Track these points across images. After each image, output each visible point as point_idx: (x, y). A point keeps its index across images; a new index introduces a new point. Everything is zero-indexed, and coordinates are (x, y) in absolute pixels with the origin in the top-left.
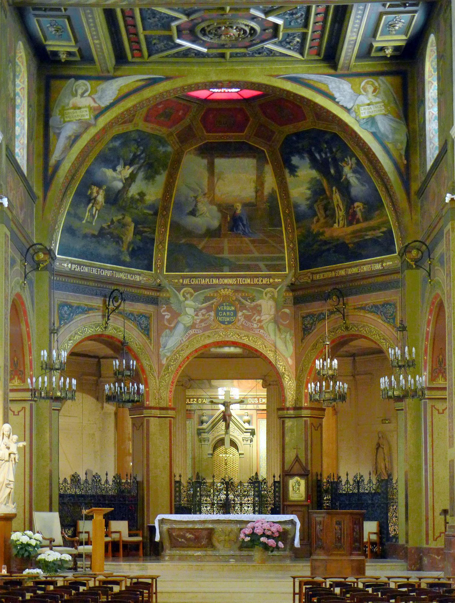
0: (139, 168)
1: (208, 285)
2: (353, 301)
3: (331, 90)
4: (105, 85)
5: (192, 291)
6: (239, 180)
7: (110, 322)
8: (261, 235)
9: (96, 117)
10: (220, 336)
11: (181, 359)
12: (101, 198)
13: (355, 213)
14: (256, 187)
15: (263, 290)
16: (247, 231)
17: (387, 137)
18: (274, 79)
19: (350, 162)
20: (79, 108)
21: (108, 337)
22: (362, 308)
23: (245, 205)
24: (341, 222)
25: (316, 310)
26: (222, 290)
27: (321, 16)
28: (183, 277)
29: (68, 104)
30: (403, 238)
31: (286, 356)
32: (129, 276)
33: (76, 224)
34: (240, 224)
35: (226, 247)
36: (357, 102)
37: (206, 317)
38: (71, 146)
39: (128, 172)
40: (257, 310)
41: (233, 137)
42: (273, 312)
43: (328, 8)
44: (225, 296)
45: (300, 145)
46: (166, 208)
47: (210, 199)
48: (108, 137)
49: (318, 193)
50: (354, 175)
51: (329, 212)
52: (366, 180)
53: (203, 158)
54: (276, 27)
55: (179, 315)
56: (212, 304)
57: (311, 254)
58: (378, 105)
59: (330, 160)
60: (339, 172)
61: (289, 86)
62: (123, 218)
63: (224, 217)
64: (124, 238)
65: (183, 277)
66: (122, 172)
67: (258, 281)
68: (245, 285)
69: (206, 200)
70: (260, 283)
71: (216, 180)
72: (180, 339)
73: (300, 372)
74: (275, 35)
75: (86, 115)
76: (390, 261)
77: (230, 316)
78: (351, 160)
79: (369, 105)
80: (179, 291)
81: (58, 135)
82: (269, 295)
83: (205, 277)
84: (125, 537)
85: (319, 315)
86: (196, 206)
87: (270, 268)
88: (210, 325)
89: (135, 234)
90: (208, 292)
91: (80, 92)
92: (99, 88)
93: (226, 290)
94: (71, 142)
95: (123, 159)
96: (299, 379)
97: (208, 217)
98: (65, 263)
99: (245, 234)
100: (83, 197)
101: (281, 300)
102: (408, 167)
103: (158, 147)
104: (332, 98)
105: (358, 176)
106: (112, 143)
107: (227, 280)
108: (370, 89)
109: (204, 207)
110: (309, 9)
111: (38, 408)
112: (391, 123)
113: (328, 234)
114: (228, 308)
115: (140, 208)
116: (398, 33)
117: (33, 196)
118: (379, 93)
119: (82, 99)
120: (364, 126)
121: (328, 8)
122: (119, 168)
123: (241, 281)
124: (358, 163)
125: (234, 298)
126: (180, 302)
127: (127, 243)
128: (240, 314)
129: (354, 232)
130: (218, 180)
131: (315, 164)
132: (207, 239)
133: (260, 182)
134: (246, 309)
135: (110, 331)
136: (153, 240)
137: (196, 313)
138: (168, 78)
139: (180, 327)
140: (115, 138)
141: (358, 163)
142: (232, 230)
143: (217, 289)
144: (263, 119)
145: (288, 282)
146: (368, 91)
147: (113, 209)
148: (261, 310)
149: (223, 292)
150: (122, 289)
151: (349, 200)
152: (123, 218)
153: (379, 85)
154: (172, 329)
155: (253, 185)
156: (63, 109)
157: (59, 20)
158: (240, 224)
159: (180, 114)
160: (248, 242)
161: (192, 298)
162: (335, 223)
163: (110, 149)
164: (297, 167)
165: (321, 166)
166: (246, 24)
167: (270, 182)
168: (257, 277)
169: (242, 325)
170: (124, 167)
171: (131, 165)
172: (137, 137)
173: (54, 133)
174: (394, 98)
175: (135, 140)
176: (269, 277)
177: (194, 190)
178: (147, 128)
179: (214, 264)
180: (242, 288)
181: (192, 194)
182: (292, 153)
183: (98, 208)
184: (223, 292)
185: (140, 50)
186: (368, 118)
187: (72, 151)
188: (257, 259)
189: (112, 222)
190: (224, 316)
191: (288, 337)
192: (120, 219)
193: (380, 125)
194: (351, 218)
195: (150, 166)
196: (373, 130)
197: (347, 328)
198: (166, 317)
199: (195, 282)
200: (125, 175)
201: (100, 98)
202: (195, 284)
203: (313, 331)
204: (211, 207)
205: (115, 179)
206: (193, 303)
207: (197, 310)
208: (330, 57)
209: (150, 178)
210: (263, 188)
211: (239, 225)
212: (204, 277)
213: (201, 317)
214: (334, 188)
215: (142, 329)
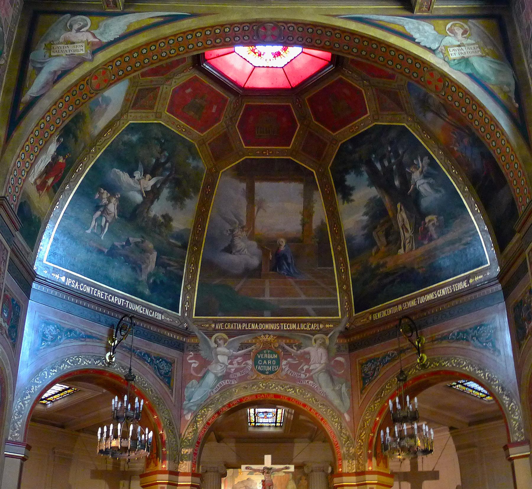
0: (164, 183)
1: (245, 330)
3: (408, 31)
5: (225, 336)
8: (309, 275)
10: (260, 387)
12: (112, 208)
14: (303, 220)
15: (311, 336)
16: (292, 271)
17: (489, 79)
18: (334, 19)
19: (421, 165)
20: (73, 43)
21: (112, 375)
23: (290, 241)
24: (407, 246)
25: (378, 353)
26: (262, 336)
28: (216, 322)
29: (58, 39)
31: (342, 411)
32: (147, 311)
34: (285, 263)
35: (268, 292)
36: (443, 43)
37: (242, 365)
38: (55, 82)
39: (149, 183)
40: (306, 358)
42: (324, 360)
44: (265, 343)
45: (356, 156)
46: (197, 243)
47: (248, 234)
49: (378, 214)
50: (426, 181)
51: (393, 237)
53: (241, 181)
56: (250, 351)
58: (472, 46)
59: (394, 167)
60: (406, 181)
61: (353, 26)
62: (143, 242)
63: (265, 254)
64: (143, 266)
65: (216, 322)
66: (142, 181)
67: (306, 327)
68: (290, 330)
69: (244, 234)
70: (308, 328)
71: (256, 209)
72: (210, 390)
73: (360, 429)
75: (81, 50)
77: (272, 365)
78: (422, 161)
79: (459, 46)
80: (210, 337)
81: (40, 70)
82: (318, 342)
83: (241, 322)
85: (384, 358)
86: (232, 241)
88: (248, 374)
90: (246, 338)
91: (76, 27)
92: (102, 25)
93: (267, 336)
94: (56, 78)
95: (143, 163)
97: (247, 254)
99: (289, 274)
101: (334, 348)
103: (187, 158)
104: (411, 39)
105: (431, 181)
106: (128, 135)
108: (460, 32)
109: (241, 243)
112: (491, 65)
113: (391, 264)
114: (270, 356)
115: (164, 234)
118: (471, 35)
119: (78, 33)
120: (457, 67)
122: (138, 175)
123: (285, 327)
125: (277, 345)
127: (147, 273)
128: (284, 362)
130: (258, 210)
131: (376, 179)
132: (244, 280)
133: (307, 214)
134: (292, 357)
137: (229, 361)
138: (193, 15)
139: (210, 379)
141: (432, 163)
142: (274, 269)
143: (256, 335)
145: (341, 328)
146: (456, 34)
148: (310, 359)
152: (143, 242)
153: (469, 27)
155: (300, 217)
156: (51, 43)
158: (285, 263)
159: (214, 110)
160: (293, 283)
161: (226, 344)
162: (400, 248)
163: (124, 143)
164: (352, 189)
168: (305, 322)
169: (286, 374)
170: (145, 175)
171: (153, 176)
172: (160, 135)
173: (34, 68)
174: (491, 40)
175: (158, 139)
176: (319, 322)
177: (231, 223)
180: (286, 334)
181: (228, 227)
183: (110, 220)
186: (460, 59)
187: (55, 87)
189: (128, 242)
190: (265, 365)
191: (344, 389)
192: (139, 242)
193: (476, 65)
195: (177, 183)
196: (469, 71)
198: (193, 365)
199: (230, 327)
200: (145, 186)
201: (101, 34)
202: (229, 330)
203: (376, 377)
204: (250, 242)
205: (132, 189)
206: (226, 351)
207: (231, 358)
209: (178, 199)
210: (311, 221)
211: (283, 263)
212: (239, 321)
213: (236, 366)
214: (399, 205)
215: (161, 375)
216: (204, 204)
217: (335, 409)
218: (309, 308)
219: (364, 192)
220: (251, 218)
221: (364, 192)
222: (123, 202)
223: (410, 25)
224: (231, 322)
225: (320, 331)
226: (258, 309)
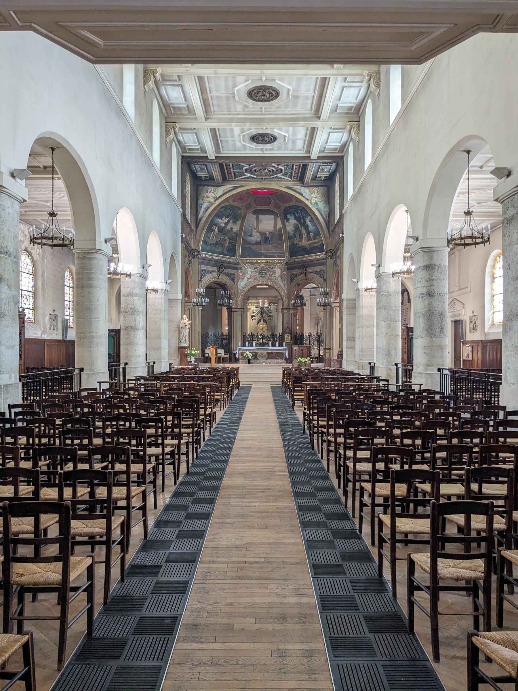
2: (309, 269)
4: (219, 188)
6: (268, 224)
7: (220, 277)
9: (215, 201)
11: (246, 290)
12: (216, 230)
13: (310, 237)
22: (312, 272)
27: (297, 167)
28: (247, 260)
30: (327, 247)
33: (207, 240)
35: (263, 249)
41: (265, 207)
43: (300, 165)
44: (263, 267)
46: (240, 234)
48: (220, 207)
49: (296, 228)
51: (301, 237)
52: (314, 225)
54: (282, 170)
55: (245, 274)
57: (294, 251)
60: (305, 221)
61: (286, 190)
63: (262, 237)
65: (247, 260)
74: (281, 172)
75: (212, 200)
76: (322, 255)
83: (255, 260)
84: (223, 356)
87: (279, 257)
89: (229, 243)
90: (256, 266)
96: (289, 298)
97: (256, 237)
98: (204, 255)
100: (210, 230)
101: (283, 269)
102: (329, 221)
104: (302, 195)
107: (263, 261)
109: (254, 233)
110: (293, 165)
111: (194, 309)
116: (326, 172)
117: (192, 231)
121: (300, 165)
122: (223, 219)
123: (268, 261)
124: (312, 218)
126: (246, 269)
129: (309, 244)
131: (296, 218)
135: (220, 280)
136: (236, 246)
138: (242, 186)
139: (246, 278)
140: (222, 208)
141: (312, 218)
142: (265, 242)
144: (277, 201)
145: (285, 262)
147: (221, 234)
149: (261, 265)
150: (224, 264)
151: (308, 232)
154: (243, 279)
156: (203, 197)
157: (202, 166)
165: (297, 219)
166: (270, 168)
167: (279, 224)
176: (279, 260)
177: (251, 227)
178: (234, 204)
179: (259, 255)
181: (250, 228)
182: (287, 214)
184: (261, 265)
185: (232, 176)
188: (273, 253)
194: (309, 239)
195: (235, 218)
197: (306, 279)
199: (251, 261)
205: (222, 223)
208: (301, 179)
209: (235, 222)
212: (254, 260)
216: (243, 222)
217: (282, 289)
218: (276, 255)
219: (293, 221)
220: (258, 225)
221: (293, 221)
222: (219, 227)
223: (302, 190)
224: (252, 260)
225: (279, 263)
226: (259, 255)
